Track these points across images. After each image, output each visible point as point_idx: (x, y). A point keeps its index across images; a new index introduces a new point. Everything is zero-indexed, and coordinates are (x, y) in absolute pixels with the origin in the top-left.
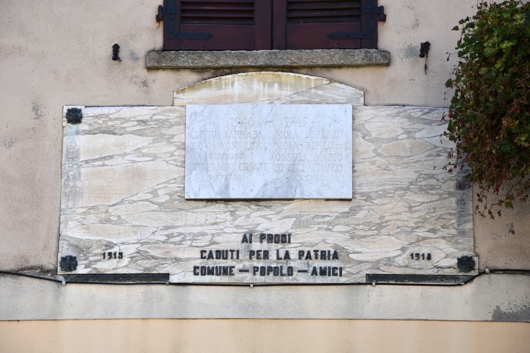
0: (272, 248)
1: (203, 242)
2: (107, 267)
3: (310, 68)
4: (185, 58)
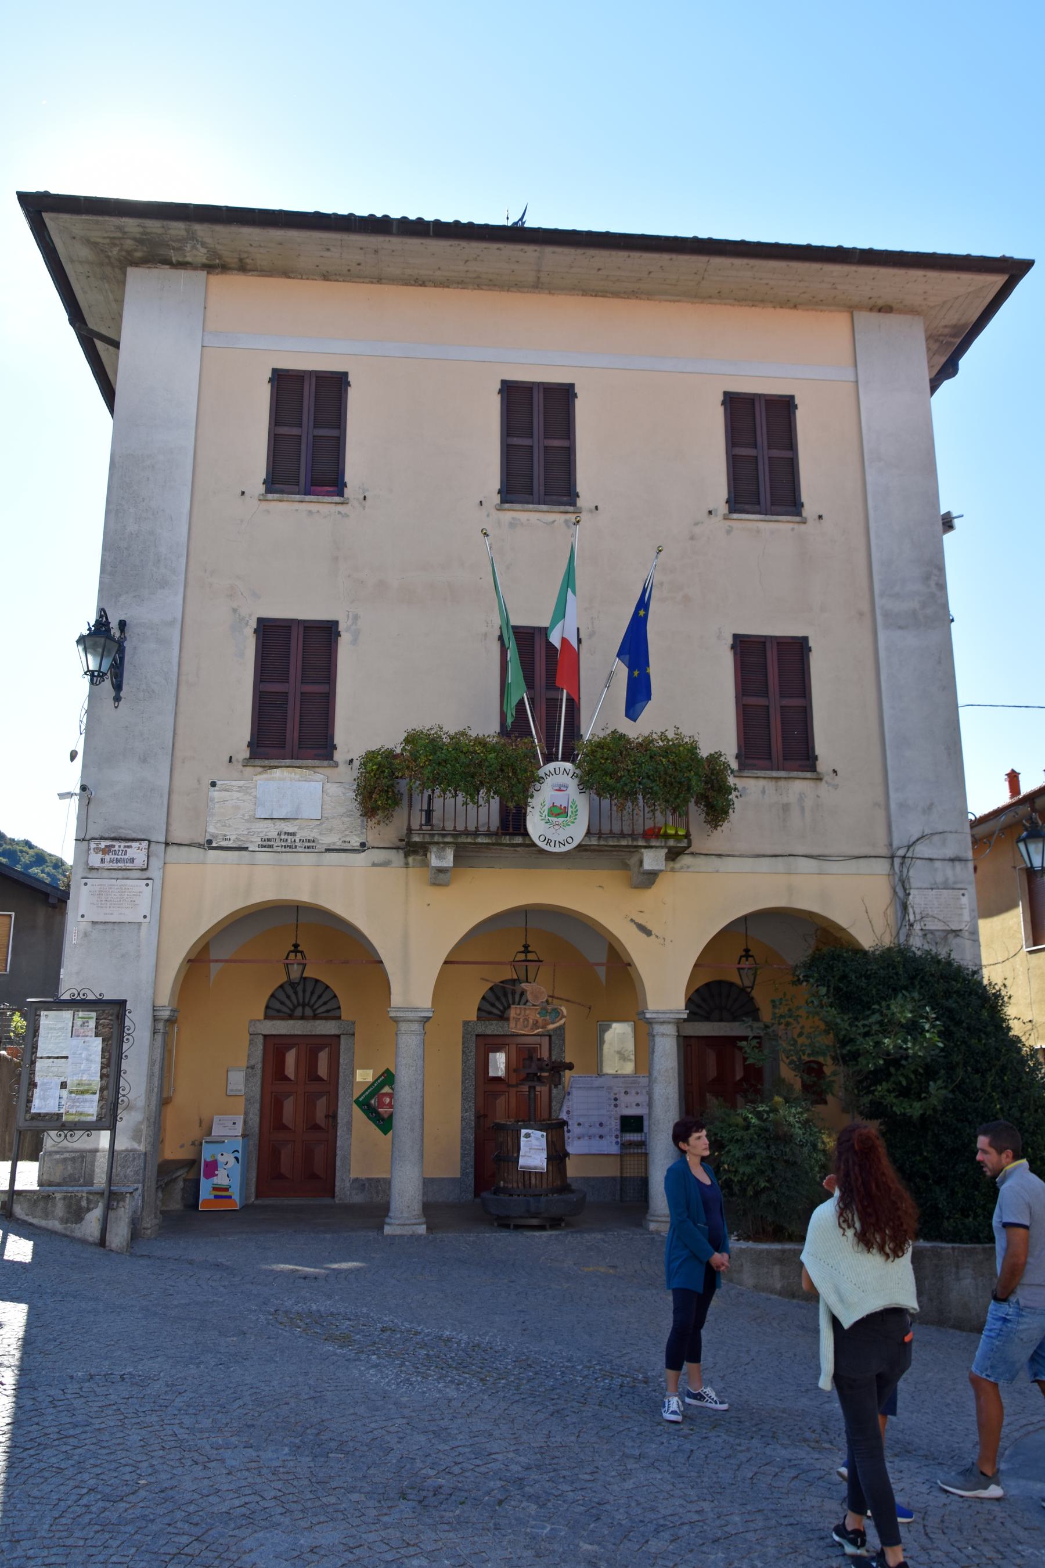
0: (289, 838)
1: (262, 835)
2: (224, 844)
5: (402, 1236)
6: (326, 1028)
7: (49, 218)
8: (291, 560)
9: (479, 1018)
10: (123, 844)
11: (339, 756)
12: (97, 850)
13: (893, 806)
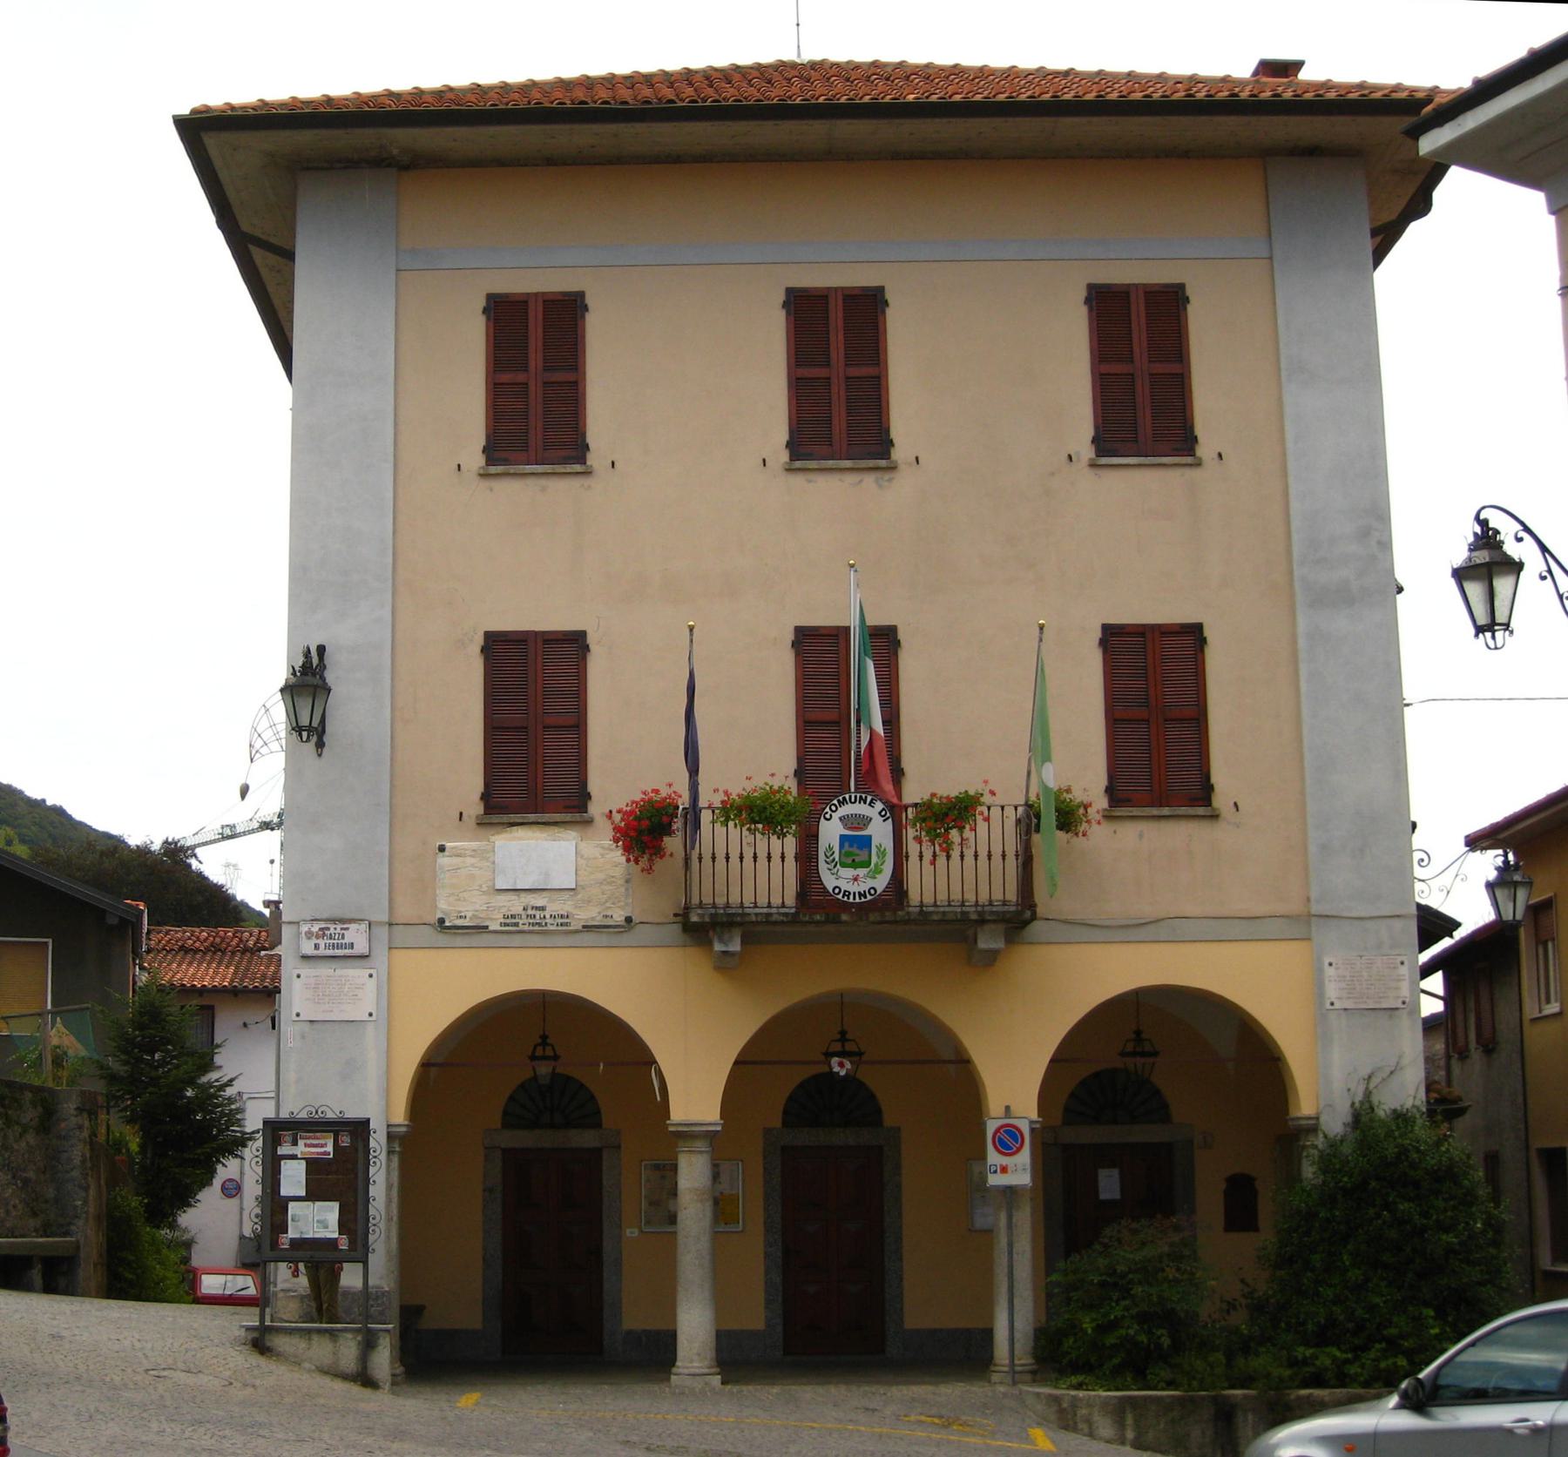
0: (538, 913)
1: (504, 910)
2: (460, 922)
3: (555, 824)
4: (495, 818)
5: (674, 1193)
6: (584, 1139)
7: (211, 141)
8: (529, 557)
9: (785, 1124)
10: (339, 927)
11: (596, 809)
12: (309, 935)
13: (1312, 848)
